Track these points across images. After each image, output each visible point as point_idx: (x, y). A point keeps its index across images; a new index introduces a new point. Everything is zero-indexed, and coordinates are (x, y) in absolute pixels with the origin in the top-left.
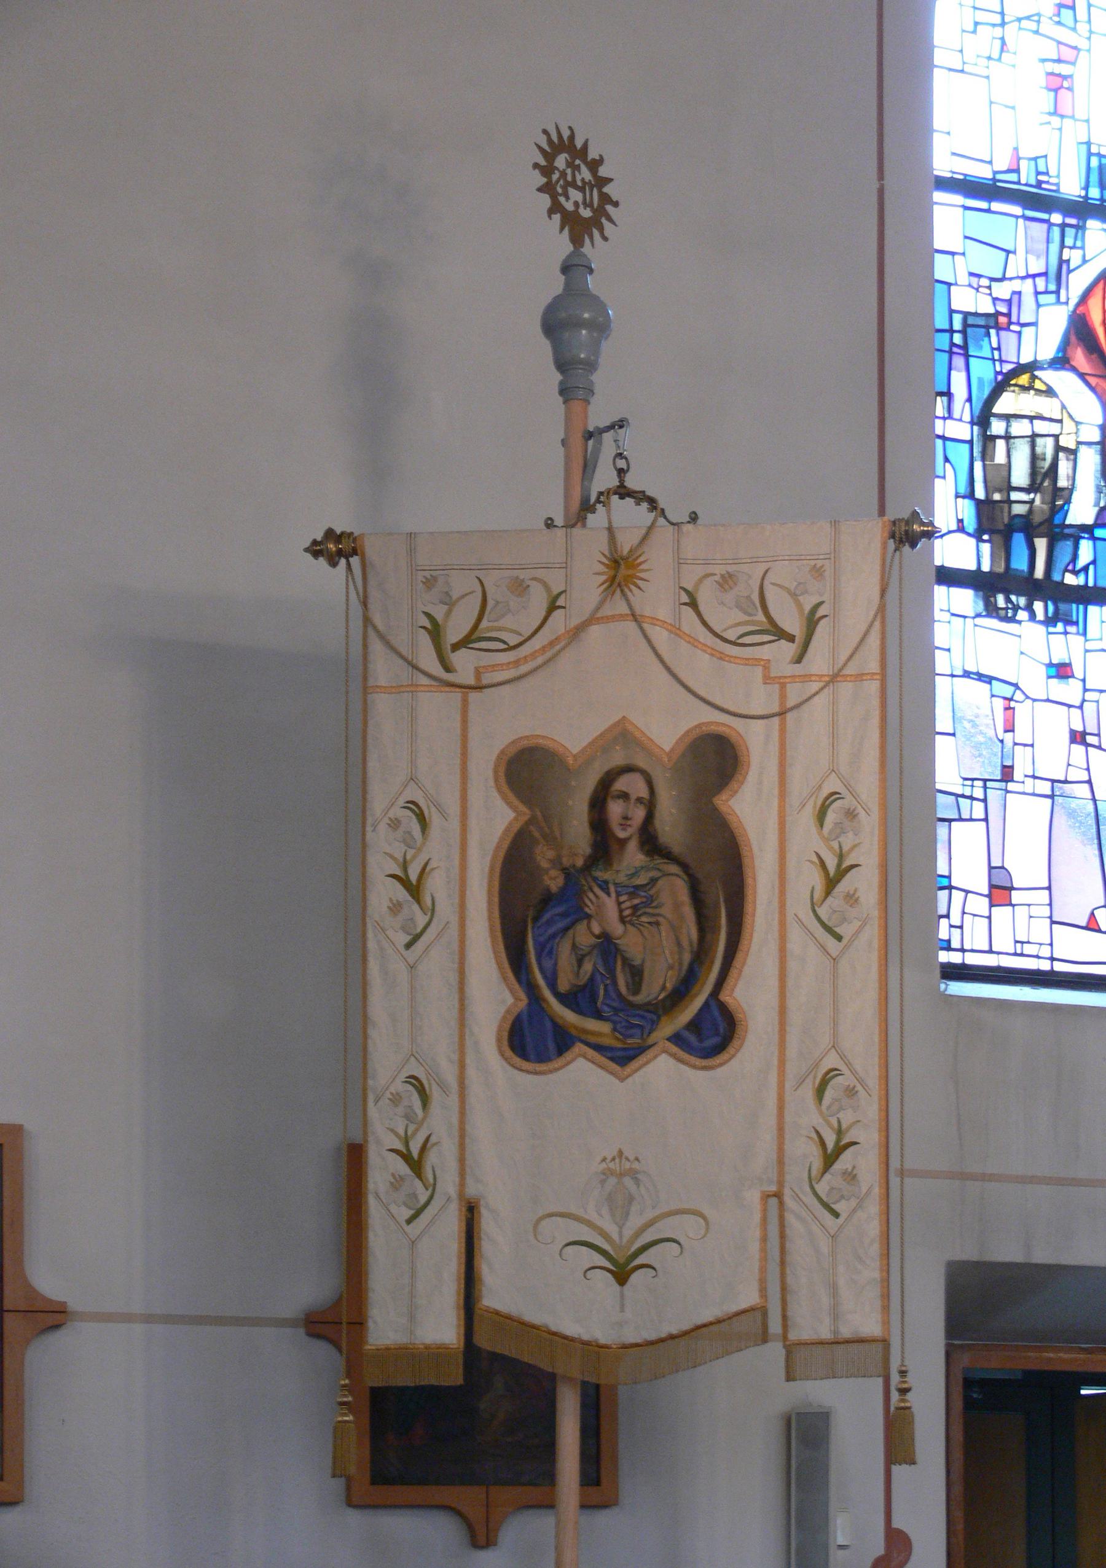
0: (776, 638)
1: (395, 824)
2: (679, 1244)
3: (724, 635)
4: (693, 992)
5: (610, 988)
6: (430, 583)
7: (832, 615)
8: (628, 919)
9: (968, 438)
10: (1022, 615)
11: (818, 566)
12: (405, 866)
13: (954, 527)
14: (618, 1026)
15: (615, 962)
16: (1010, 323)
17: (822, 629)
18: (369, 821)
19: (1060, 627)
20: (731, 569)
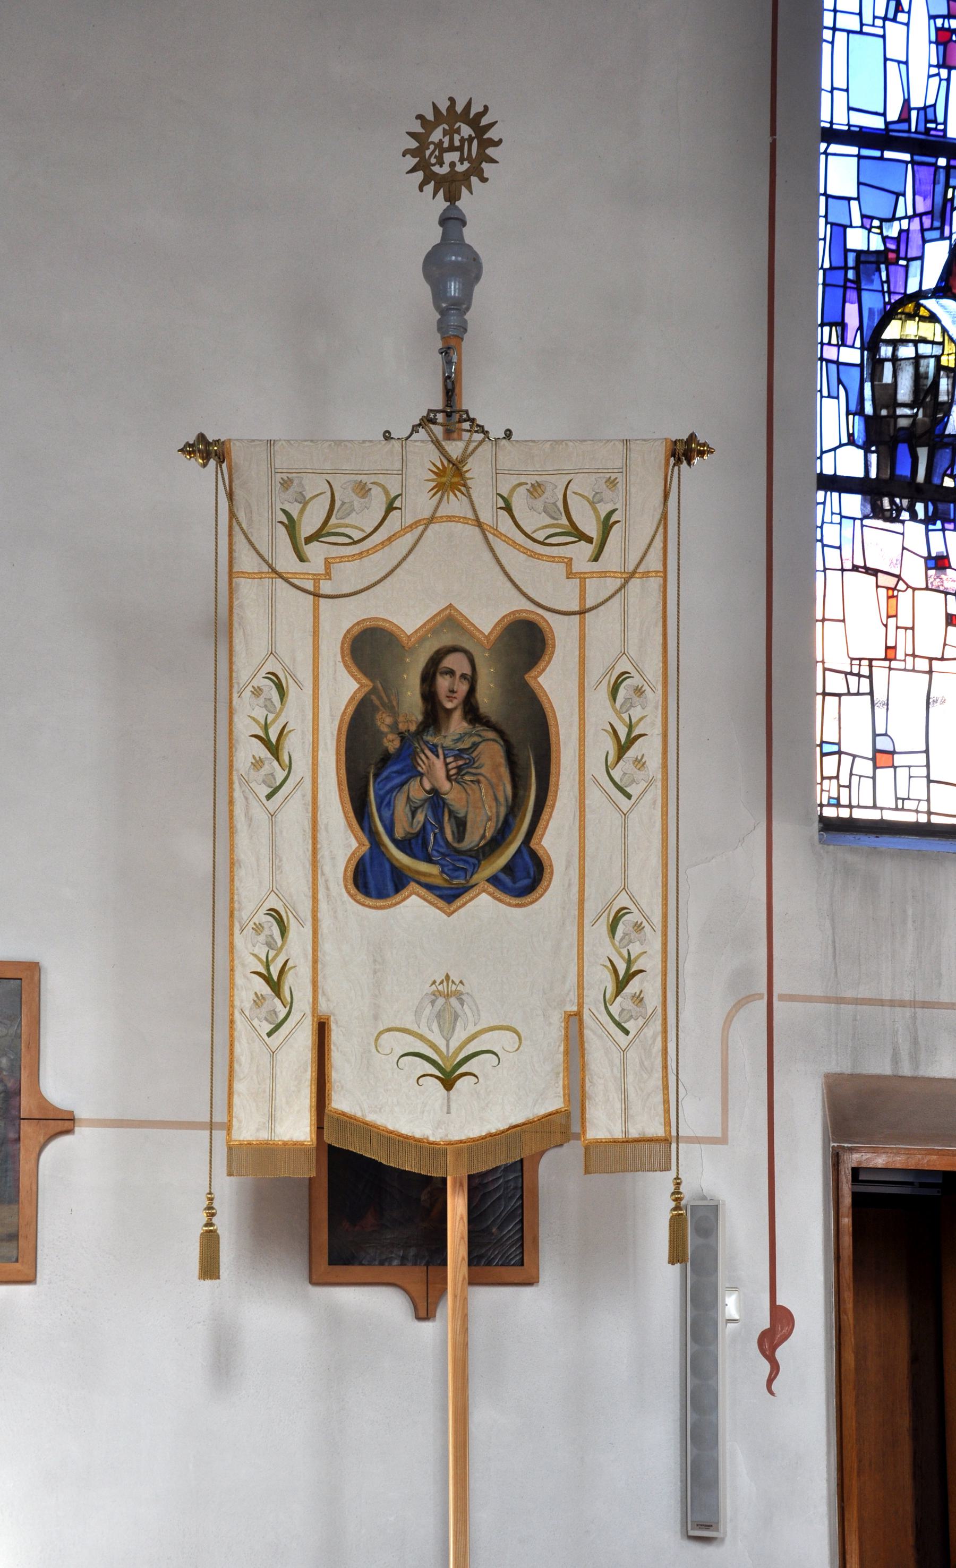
0: (577, 539)
1: (257, 692)
2: (497, 1055)
3: (534, 536)
4: (508, 840)
5: (439, 836)
6: (286, 484)
7: (624, 521)
8: (454, 777)
9: (858, 361)
10: (905, 515)
11: (612, 479)
12: (266, 728)
13: (845, 440)
14: (446, 869)
15: (443, 815)
16: (899, 258)
17: (615, 532)
18: (235, 690)
19: (939, 525)
20: (538, 479)
